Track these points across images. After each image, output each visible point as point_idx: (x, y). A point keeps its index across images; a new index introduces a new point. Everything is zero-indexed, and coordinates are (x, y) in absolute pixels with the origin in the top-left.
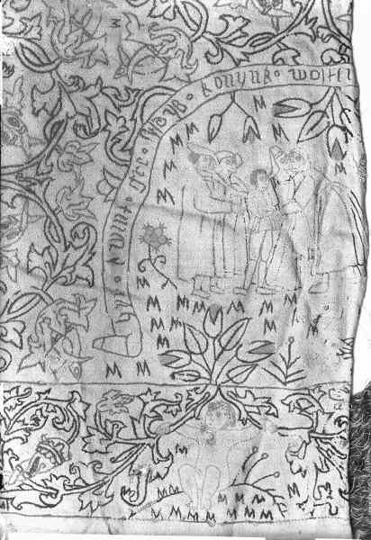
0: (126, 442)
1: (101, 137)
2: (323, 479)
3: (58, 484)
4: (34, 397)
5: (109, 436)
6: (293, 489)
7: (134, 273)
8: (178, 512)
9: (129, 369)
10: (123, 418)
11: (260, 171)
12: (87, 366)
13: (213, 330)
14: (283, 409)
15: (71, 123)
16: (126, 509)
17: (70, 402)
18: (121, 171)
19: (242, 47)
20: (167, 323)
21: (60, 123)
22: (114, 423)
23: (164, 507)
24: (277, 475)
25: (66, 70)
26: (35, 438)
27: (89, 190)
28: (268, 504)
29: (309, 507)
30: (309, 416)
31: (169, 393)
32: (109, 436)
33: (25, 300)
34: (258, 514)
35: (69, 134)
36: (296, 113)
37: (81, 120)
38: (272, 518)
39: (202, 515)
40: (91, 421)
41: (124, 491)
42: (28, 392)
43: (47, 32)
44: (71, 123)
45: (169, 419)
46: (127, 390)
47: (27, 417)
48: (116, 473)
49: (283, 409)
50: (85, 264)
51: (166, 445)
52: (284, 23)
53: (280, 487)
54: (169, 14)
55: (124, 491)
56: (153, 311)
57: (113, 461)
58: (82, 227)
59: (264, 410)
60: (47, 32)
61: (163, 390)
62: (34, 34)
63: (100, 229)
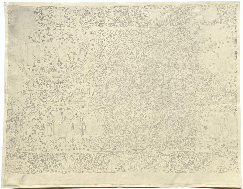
0: (202, 160)
1: (197, 112)
2: (235, 166)
3: (192, 167)
4: (86, 154)
5: (200, 159)
6: (230, 167)
7: (203, 133)
8: (211, 171)
9: (202, 148)
10: (202, 156)
11: (222, 117)
12: (196, 148)
13: (215, 142)
14: (227, 155)
15: (192, 110)
16: (203, 171)
17: (193, 154)
18: (200, 118)
19: (161, 159)
20: (208, 141)
21: (191, 110)
22: (201, 157)
23: (209, 170)
24: (227, 165)
25: (192, 102)
26: (188, 160)
27: (195, 120)
28: (226, 169)
29: (232, 170)
30: (231, 156)
31: (209, 152)
32: (200, 159)
33: (186, 138)
34: (224, 171)
35: (192, 112)
36: (228, 108)
37: (194, 109)
38: (7, 108)
39: (215, 171)
40: (197, 157)
41: (203, 168)
42: (187, 153)
43: (189, 96)
44: (192, 110)
45: (209, 156)
46: (202, 152)
47: (187, 157)
48: (201, 165)
49: (227, 155)
50: (195, 132)
51: (209, 160)
52: (227, 93)
53: (228, 166)
54: (208, 92)
55: (203, 168)
56: (206, 139)
57: (201, 163)
58: (194, 126)
59: (224, 155)
60: (189, 96)
61: (208, 152)
62: (187, 96)
63: (197, 127)
